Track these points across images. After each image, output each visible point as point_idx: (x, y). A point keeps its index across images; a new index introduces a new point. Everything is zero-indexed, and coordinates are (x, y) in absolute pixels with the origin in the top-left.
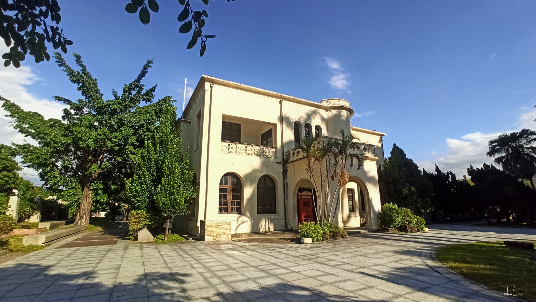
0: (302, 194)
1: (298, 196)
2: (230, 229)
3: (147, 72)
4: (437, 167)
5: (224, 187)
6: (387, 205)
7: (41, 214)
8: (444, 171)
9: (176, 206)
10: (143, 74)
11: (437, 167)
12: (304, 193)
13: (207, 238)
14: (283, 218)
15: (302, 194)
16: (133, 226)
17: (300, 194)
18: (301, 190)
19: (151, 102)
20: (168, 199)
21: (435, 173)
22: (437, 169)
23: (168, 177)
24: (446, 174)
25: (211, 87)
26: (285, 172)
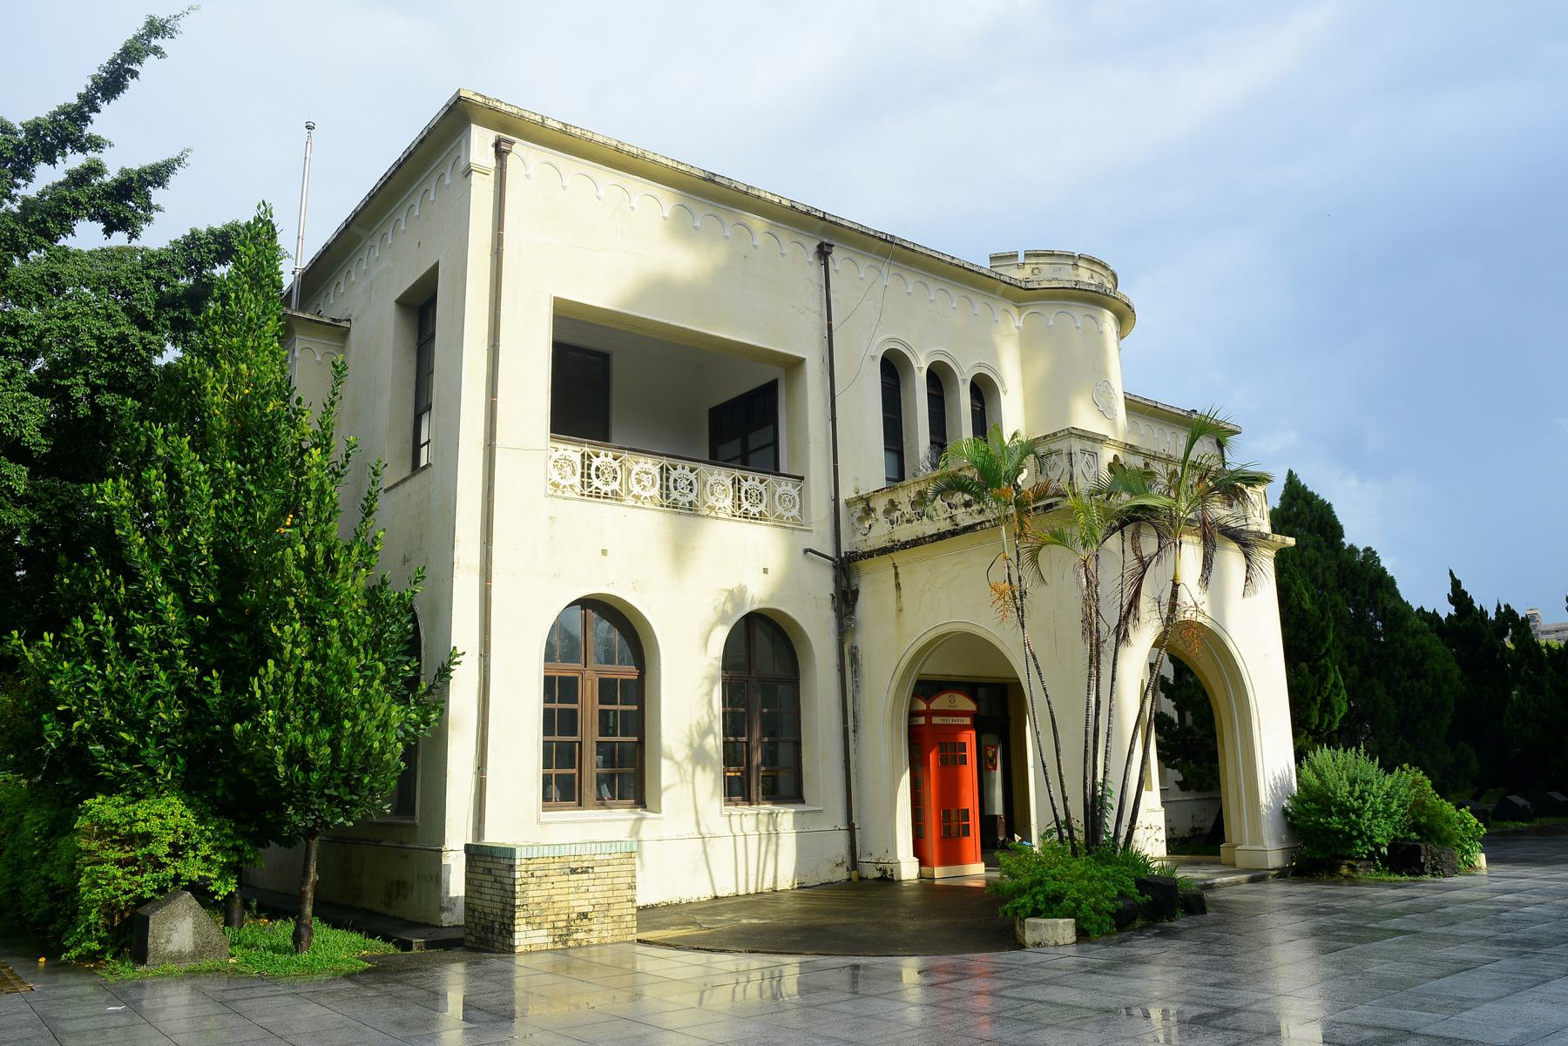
0: (935, 705)
1: (913, 714)
2: (632, 887)
3: (134, 74)
4: (1456, 584)
5: (567, 669)
6: (1322, 755)
7: (1399, 614)
8: (1486, 600)
9: (364, 771)
10: (112, 83)
11: (1456, 584)
12: (941, 703)
13: (524, 936)
14: (842, 824)
15: (935, 705)
16: (107, 880)
17: (922, 706)
18: (926, 688)
19: (133, 236)
20: (326, 734)
21: (1446, 610)
22: (1459, 596)
23: (310, 620)
24: (1492, 615)
25: (500, 153)
26: (845, 600)
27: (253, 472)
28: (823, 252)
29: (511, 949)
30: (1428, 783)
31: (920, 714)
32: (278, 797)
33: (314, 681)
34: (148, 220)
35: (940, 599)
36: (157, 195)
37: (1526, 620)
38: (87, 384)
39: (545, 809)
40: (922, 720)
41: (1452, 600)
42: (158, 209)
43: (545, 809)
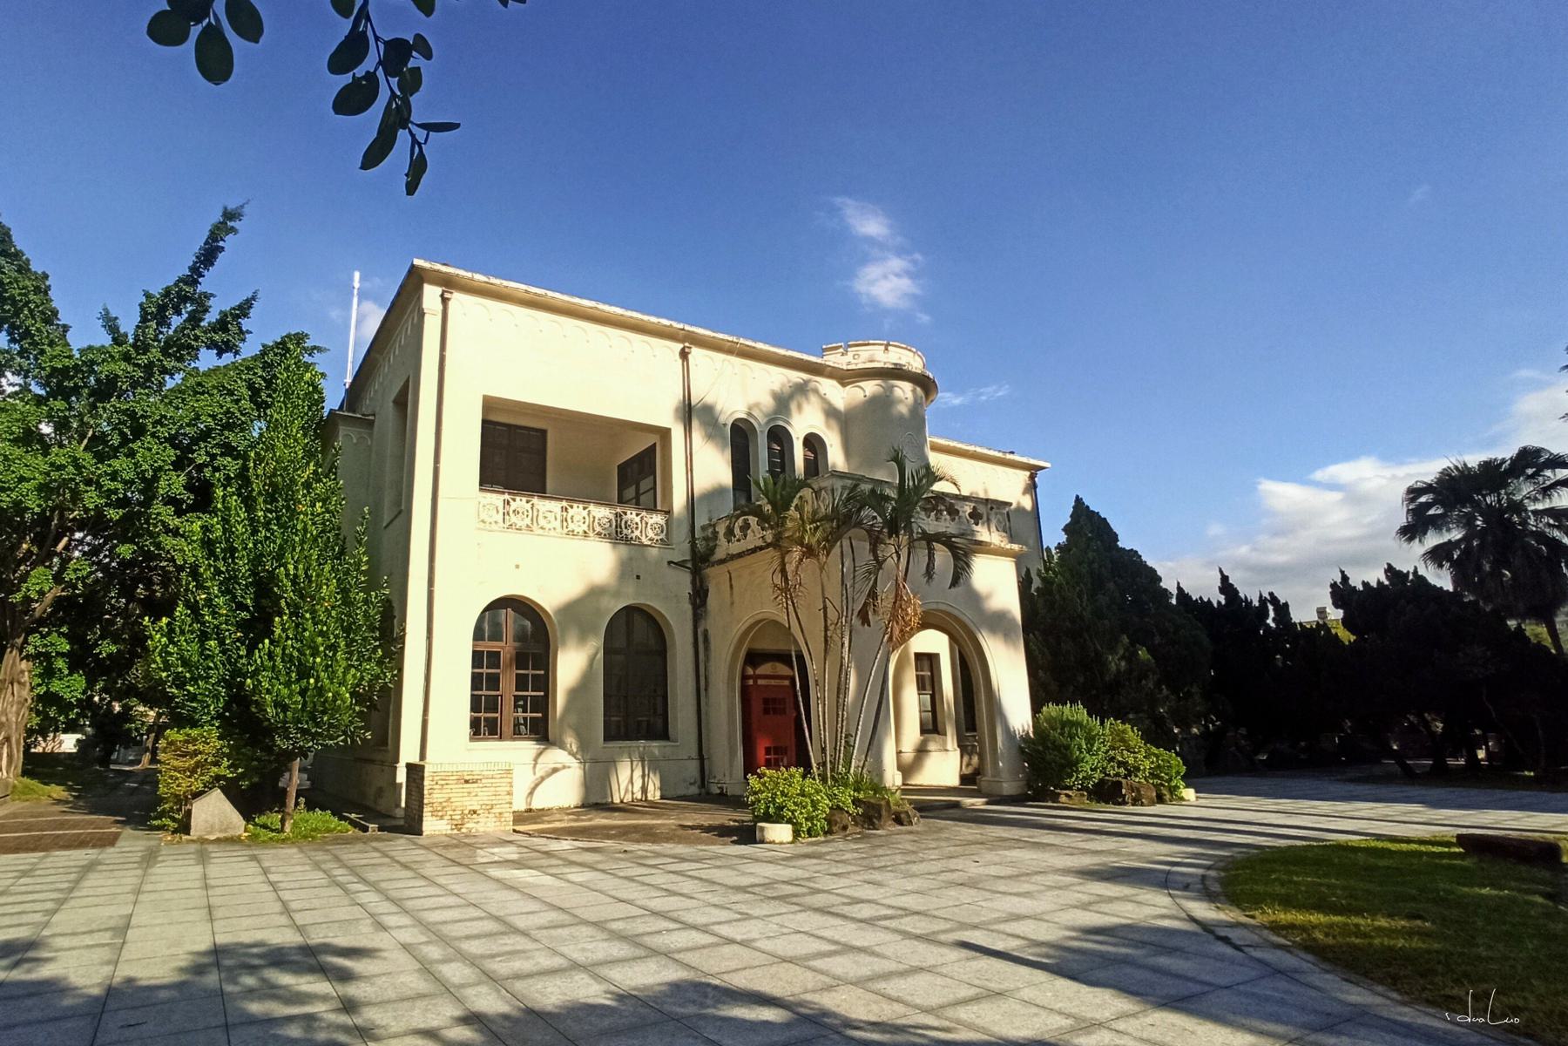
0: (759, 671)
1: (744, 677)
2: (509, 793)
4: (1225, 579)
5: (488, 646)
6: (1050, 710)
8: (1250, 592)
9: (324, 712)
10: (209, 255)
11: (1225, 579)
13: (430, 825)
15: (759, 671)
17: (750, 671)
18: (754, 658)
21: (1217, 598)
22: (1226, 587)
25: (445, 301)
26: (699, 597)
27: (278, 518)
28: (684, 355)
29: (420, 833)
30: (1133, 735)
31: (750, 677)
32: (269, 731)
33: (296, 654)
34: (244, 340)
35: (748, 599)
36: (245, 324)
37: (1286, 605)
38: (207, 453)
39: (471, 739)
40: (751, 682)
41: (1222, 590)
42: (249, 332)
43: (471, 739)
